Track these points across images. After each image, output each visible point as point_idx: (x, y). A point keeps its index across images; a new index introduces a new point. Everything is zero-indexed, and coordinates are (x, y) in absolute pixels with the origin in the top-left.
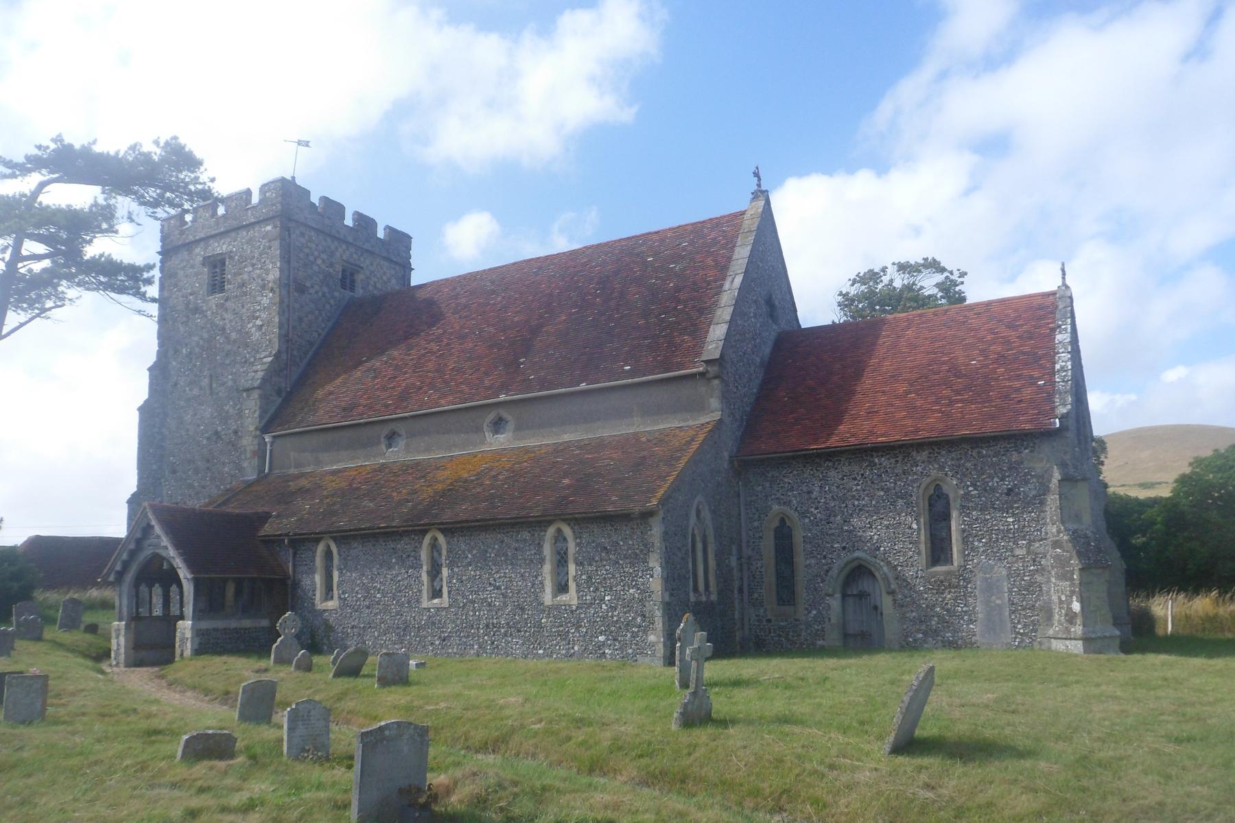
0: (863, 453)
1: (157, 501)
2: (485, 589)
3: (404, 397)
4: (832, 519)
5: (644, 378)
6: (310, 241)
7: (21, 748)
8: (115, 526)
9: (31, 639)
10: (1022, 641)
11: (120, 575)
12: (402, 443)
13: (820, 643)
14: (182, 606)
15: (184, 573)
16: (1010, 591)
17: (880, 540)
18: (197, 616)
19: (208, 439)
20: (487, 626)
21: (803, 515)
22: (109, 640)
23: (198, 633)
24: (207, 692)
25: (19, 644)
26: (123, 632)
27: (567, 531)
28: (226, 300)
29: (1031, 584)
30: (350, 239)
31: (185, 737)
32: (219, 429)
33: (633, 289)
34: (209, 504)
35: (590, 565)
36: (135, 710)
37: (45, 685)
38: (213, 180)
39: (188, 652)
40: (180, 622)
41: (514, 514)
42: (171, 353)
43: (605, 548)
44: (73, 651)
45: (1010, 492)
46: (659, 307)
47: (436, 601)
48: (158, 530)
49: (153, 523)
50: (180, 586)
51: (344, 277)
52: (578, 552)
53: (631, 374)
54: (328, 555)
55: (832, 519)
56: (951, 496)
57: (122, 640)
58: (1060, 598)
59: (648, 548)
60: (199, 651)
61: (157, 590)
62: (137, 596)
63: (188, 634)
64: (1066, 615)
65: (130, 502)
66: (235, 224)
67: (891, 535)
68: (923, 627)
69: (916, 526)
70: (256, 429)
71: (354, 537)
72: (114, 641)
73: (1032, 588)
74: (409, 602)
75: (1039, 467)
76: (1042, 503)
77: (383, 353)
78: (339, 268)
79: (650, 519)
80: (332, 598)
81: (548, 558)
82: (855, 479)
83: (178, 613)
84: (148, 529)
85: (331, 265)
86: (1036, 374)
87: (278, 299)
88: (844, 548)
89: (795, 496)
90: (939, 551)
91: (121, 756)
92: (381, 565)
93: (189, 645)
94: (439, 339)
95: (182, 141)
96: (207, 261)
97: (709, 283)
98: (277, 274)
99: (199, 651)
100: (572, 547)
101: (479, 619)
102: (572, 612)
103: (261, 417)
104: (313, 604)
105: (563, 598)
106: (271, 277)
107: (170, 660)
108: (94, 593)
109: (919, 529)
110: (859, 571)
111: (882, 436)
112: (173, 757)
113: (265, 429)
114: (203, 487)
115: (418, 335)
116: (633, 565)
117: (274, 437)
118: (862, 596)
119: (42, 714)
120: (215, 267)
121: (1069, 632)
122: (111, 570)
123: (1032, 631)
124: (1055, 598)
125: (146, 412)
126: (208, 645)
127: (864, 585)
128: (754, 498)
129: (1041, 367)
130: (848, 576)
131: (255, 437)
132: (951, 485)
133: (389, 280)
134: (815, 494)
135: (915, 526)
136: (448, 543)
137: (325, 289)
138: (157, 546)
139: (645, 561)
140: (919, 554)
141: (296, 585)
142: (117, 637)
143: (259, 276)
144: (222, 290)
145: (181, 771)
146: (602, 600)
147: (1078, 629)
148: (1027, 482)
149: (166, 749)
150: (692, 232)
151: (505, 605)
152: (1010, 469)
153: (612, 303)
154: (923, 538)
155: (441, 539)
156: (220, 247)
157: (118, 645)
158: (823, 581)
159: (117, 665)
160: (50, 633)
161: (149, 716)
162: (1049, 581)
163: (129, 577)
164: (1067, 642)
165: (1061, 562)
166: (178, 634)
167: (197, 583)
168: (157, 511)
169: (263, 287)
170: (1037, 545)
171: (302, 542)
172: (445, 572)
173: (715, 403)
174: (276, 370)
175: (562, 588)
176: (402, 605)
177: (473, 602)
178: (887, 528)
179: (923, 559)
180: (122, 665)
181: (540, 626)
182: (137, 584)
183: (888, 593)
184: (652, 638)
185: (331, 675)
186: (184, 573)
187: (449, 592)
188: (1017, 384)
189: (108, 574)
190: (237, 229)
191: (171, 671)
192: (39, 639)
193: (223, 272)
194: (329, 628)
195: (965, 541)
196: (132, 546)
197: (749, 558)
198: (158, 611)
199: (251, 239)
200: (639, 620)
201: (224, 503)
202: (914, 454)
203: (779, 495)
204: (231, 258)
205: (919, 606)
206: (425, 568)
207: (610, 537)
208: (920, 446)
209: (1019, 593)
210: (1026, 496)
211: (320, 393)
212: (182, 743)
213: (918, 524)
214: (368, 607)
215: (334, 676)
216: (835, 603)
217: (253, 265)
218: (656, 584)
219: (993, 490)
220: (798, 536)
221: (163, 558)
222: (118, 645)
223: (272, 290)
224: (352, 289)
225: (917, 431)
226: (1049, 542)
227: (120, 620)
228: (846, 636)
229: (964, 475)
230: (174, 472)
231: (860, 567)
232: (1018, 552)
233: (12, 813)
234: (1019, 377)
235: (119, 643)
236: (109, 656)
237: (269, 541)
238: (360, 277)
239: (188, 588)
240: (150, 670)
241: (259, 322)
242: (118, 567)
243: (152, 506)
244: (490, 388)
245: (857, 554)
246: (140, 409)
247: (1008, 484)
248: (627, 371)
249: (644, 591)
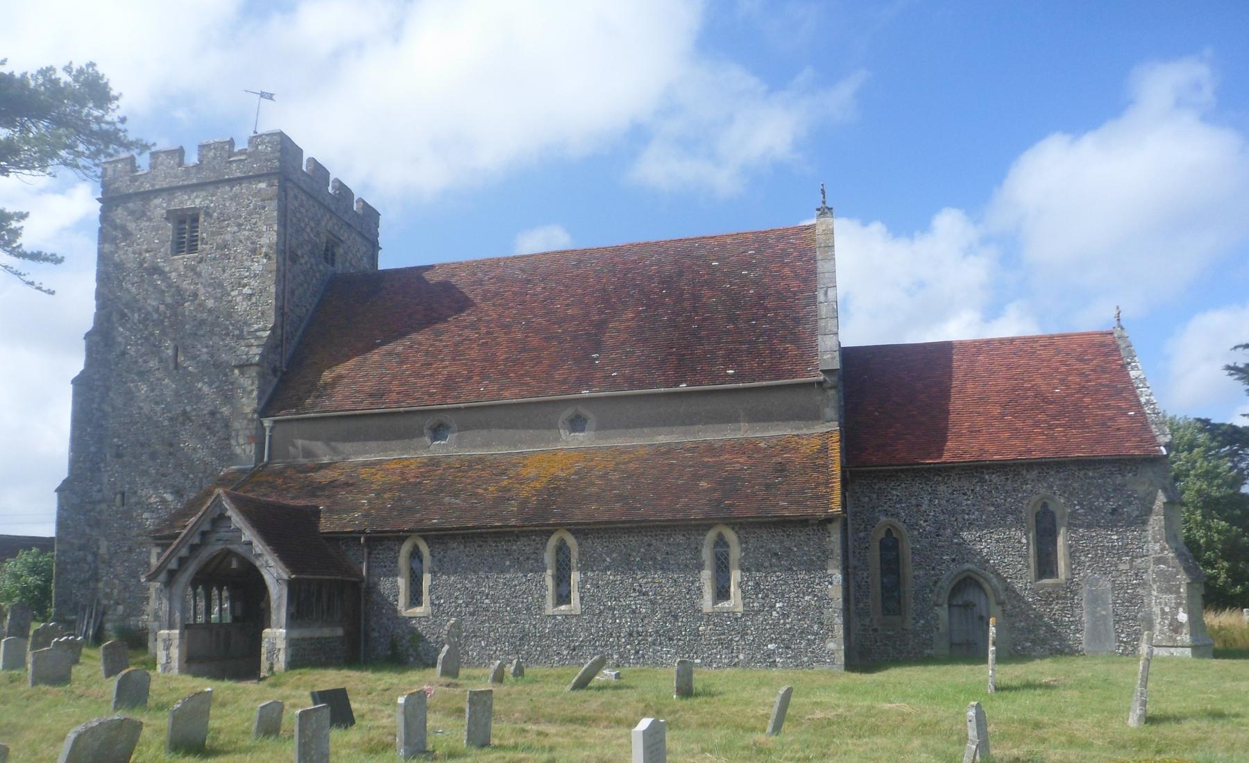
0: (976, 469)
2: (627, 595)
3: (450, 384)
4: (941, 532)
5: (764, 383)
6: (302, 205)
10: (1126, 649)
12: (451, 437)
13: (928, 651)
16: (1114, 603)
17: (991, 553)
20: (631, 635)
21: (912, 527)
23: (292, 643)
26: (176, 642)
27: (731, 536)
28: (200, 262)
29: (1134, 596)
30: (333, 207)
32: (188, 408)
33: (705, 291)
35: (758, 571)
38: (123, 120)
39: (281, 660)
41: (669, 516)
42: (115, 317)
43: (776, 554)
45: (1114, 511)
46: (712, 315)
47: (563, 607)
49: (229, 513)
51: (327, 250)
52: (745, 558)
53: (735, 379)
54: (415, 554)
55: (941, 532)
56: (1058, 515)
58: (1162, 610)
59: (826, 555)
63: (281, 644)
64: (1170, 624)
66: (212, 177)
67: (1003, 550)
68: (1032, 636)
69: (1024, 539)
70: (255, 411)
71: (454, 537)
73: (1133, 600)
74: (528, 609)
75: (1141, 490)
76: (1145, 523)
77: (402, 335)
78: (324, 239)
79: (829, 526)
80: (420, 604)
81: (707, 563)
82: (965, 494)
85: (318, 234)
86: (1123, 405)
87: (274, 267)
88: (954, 560)
89: (902, 508)
90: (1046, 566)
92: (490, 568)
94: (473, 326)
95: (101, 69)
96: (171, 215)
97: (795, 294)
98: (274, 238)
100: (735, 553)
101: (620, 626)
102: (736, 619)
103: (260, 398)
104: (395, 611)
105: (724, 605)
106: (264, 240)
109: (1028, 544)
110: (967, 583)
111: (996, 454)
113: (264, 412)
114: (164, 475)
115: (446, 321)
116: (808, 571)
117: (275, 422)
118: (968, 606)
120: (182, 222)
121: (1175, 640)
123: (1134, 640)
124: (1156, 610)
125: (82, 385)
127: (971, 595)
128: (860, 509)
129: (1126, 399)
130: (953, 589)
131: (252, 420)
132: (1059, 504)
133: (361, 258)
134: (924, 507)
135: (1024, 541)
136: (580, 545)
137: (313, 260)
139: (823, 568)
140: (1028, 567)
141: (372, 589)
142: (167, 648)
143: (248, 238)
144: (193, 249)
146: (773, 607)
147: (1185, 637)
148: (1130, 503)
150: (754, 241)
151: (654, 612)
152: (1114, 490)
153: (687, 304)
154: (1031, 552)
155: (571, 541)
156: (194, 201)
157: (168, 657)
158: (931, 591)
162: (1150, 594)
164: (1172, 650)
165: (1165, 578)
169: (254, 251)
170: (1139, 561)
171: (381, 541)
172: (575, 577)
173: (830, 412)
174: (273, 346)
175: (722, 593)
176: (519, 612)
177: (612, 609)
178: (997, 541)
179: (1032, 572)
181: (697, 634)
183: (998, 604)
184: (831, 645)
185: (568, 688)
187: (582, 599)
188: (1109, 413)
190: (217, 183)
193: (194, 228)
194: (417, 637)
195: (1072, 555)
197: (855, 567)
199: (236, 195)
200: (816, 627)
202: (1024, 472)
203: (886, 507)
204: (208, 215)
205: (1028, 616)
206: (549, 572)
207: (781, 542)
208: (1030, 465)
209: (1122, 604)
210: (1129, 516)
211: (327, 376)
213: (1027, 539)
214: (472, 614)
215: (574, 688)
216: (943, 613)
217: (239, 225)
218: (835, 590)
219: (1099, 509)
220: (907, 546)
222: (168, 657)
223: (266, 255)
224: (333, 264)
225: (1029, 451)
226: (1151, 558)
227: (171, 627)
228: (952, 645)
229: (1071, 494)
231: (969, 577)
232: (1121, 567)
234: (1107, 407)
237: (334, 538)
238: (340, 251)
241: (246, 290)
244: (564, 382)
245: (967, 566)
247: (1112, 504)
248: (732, 375)
249: (820, 599)
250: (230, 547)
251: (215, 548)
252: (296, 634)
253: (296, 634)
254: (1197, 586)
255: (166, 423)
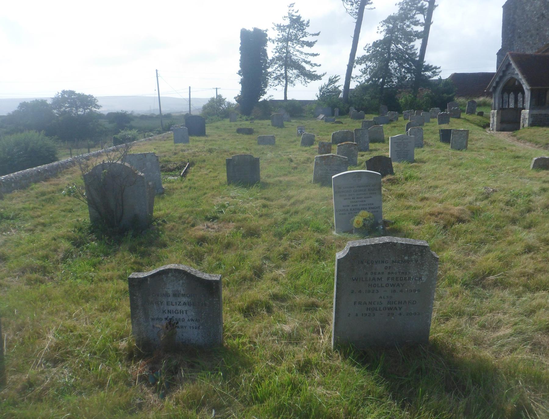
1: (512, 52)
7: (461, 159)
8: (492, 68)
9: (456, 118)
11: (495, 88)
14: (523, 103)
15: (526, 87)
18: (531, 108)
19: (538, 18)
22: (489, 118)
23: (531, 115)
24: (537, 143)
25: (451, 120)
26: (496, 115)
31: (535, 159)
32: (544, 12)
34: (538, 52)
36: (505, 148)
37: (467, 134)
39: (526, 125)
40: (523, 111)
44: (474, 123)
48: (514, 65)
49: (511, 62)
50: (523, 93)
57: (495, 119)
60: (532, 125)
61: (512, 96)
62: (502, 98)
63: (527, 117)
65: (498, 54)
72: (491, 119)
83: (521, 107)
84: (509, 65)
91: (504, 165)
93: (527, 121)
99: (532, 125)
107: (518, 128)
108: (481, 99)
112: (529, 166)
119: (466, 147)
122: (491, 86)
126: (536, 122)
138: (513, 74)
142: (493, 118)
145: (534, 173)
149: (527, 164)
157: (493, 121)
159: (493, 130)
160: (463, 115)
161: (512, 151)
163: (499, 89)
166: (522, 116)
167: (532, 91)
168: (514, 56)
180: (495, 130)
182: (503, 92)
186: (526, 87)
189: (489, 88)
191: (518, 133)
192: (459, 117)
196: (501, 74)
198: (512, 105)
201: (546, 51)
212: (533, 161)
221: (516, 80)
222: (493, 121)
230: (520, 37)
233: (464, 181)
235: (494, 120)
236: (489, 126)
239: (528, 94)
240: (508, 133)
242: (494, 85)
243: (511, 54)
246: (503, 7)
250: (513, 76)
251: (508, 77)
252: (535, 112)
253: (535, 112)
254: (157, 264)
255: (536, 20)
